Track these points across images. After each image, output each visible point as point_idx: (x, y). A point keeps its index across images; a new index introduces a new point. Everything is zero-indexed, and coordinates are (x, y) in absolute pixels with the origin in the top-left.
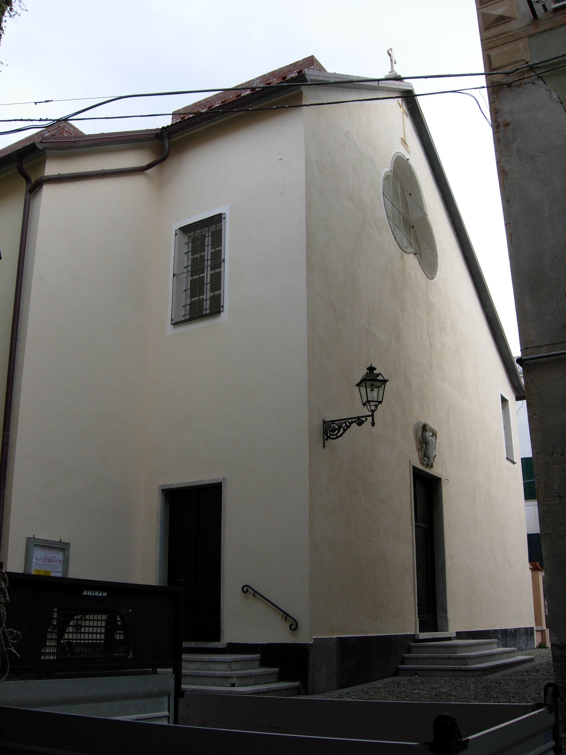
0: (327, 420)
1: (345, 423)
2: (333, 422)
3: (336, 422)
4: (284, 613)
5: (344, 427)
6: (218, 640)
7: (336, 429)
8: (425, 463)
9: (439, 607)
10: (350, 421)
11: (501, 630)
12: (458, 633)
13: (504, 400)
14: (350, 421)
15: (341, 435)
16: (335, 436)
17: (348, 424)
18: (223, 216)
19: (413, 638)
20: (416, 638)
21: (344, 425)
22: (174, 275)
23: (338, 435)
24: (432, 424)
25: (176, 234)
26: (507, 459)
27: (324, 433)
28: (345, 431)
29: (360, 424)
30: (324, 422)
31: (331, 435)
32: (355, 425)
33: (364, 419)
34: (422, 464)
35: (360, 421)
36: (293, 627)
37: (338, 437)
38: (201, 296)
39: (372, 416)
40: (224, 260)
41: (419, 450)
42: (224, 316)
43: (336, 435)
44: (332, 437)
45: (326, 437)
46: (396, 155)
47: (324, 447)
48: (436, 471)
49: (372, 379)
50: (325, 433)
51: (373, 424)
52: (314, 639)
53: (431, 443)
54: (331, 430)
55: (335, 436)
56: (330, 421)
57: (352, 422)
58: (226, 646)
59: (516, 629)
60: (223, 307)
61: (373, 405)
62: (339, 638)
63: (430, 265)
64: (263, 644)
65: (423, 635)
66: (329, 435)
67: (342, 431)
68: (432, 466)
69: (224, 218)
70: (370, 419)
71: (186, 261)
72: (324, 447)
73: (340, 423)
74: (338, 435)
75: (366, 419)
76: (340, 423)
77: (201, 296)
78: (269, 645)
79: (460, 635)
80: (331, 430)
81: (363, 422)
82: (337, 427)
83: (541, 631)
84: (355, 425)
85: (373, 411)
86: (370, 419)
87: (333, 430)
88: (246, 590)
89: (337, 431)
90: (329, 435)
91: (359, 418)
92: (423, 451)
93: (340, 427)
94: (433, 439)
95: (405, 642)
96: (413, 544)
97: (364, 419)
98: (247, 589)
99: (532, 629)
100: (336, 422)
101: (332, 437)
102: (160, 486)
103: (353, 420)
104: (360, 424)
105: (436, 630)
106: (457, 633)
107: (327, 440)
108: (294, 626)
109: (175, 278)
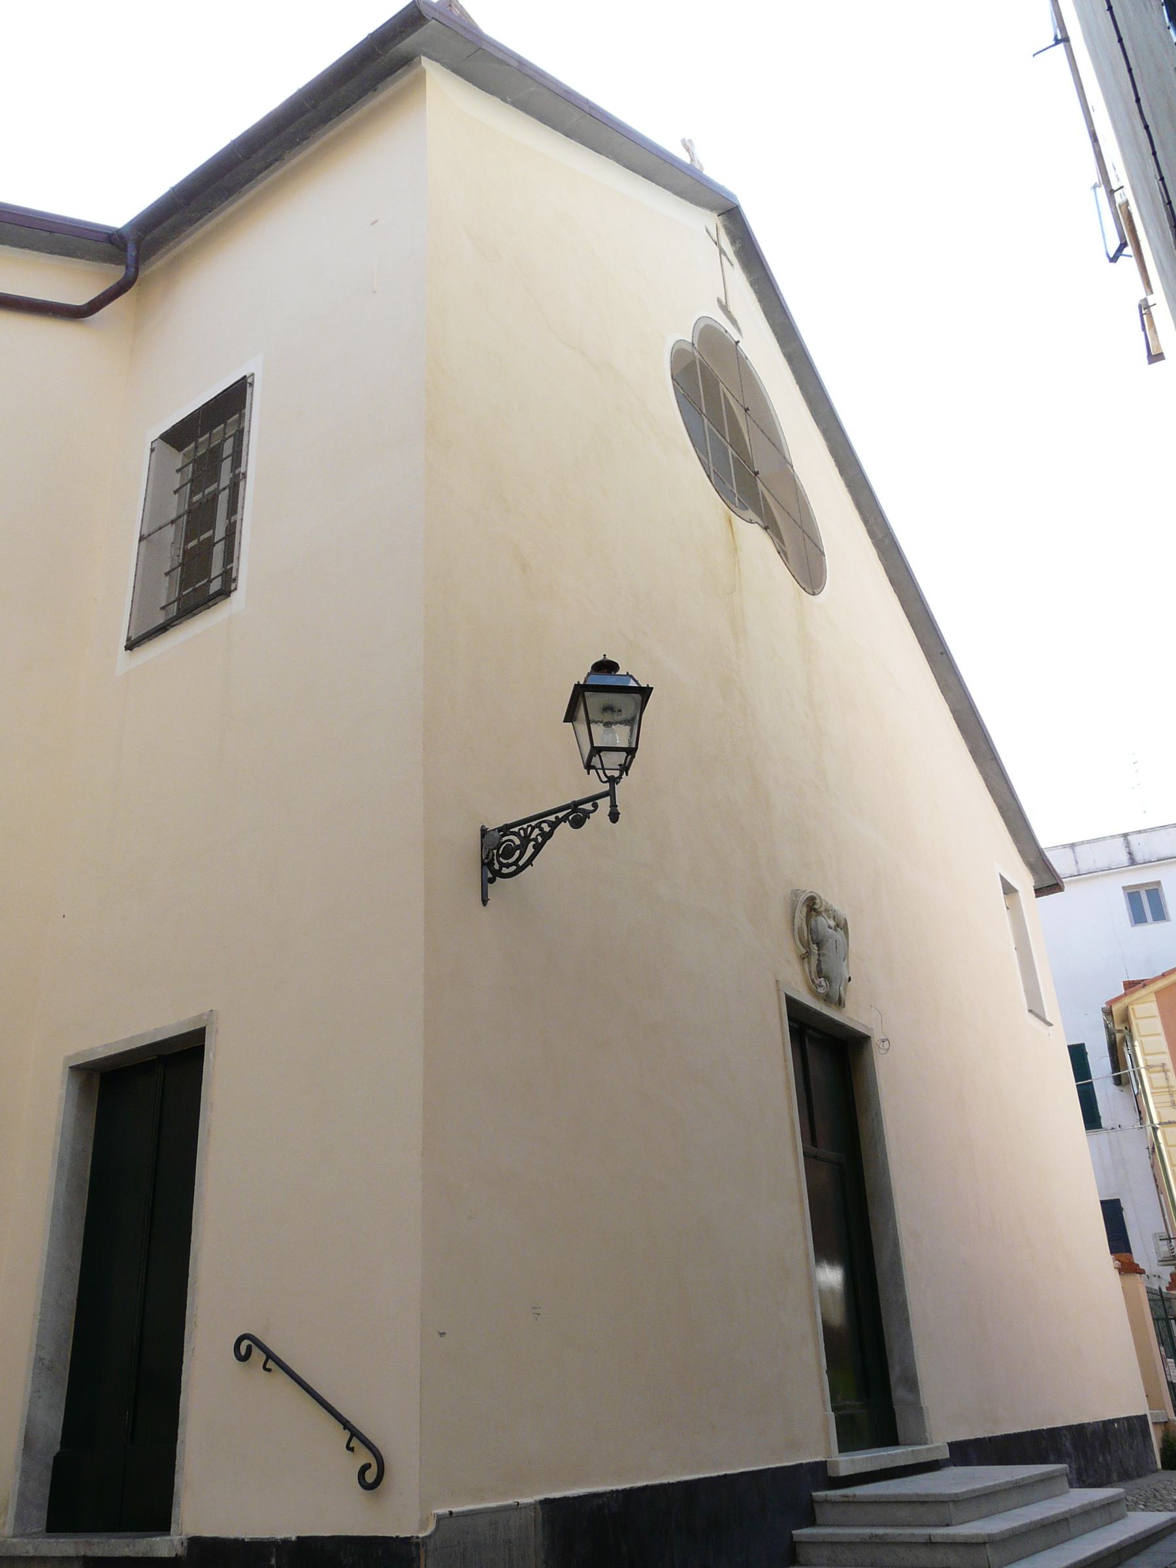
0: (491, 826)
1: (539, 826)
2: (505, 829)
3: (516, 829)
4: (346, 1424)
5: (535, 840)
6: (162, 1523)
7: (518, 847)
8: (821, 990)
9: (895, 1373)
10: (552, 818)
11: (1070, 1428)
12: (952, 1446)
13: (1009, 890)
14: (552, 818)
15: (529, 862)
16: (514, 868)
17: (546, 828)
18: (249, 380)
19: (819, 1474)
20: (831, 1473)
21: (537, 831)
22: (141, 539)
23: (521, 863)
24: (830, 897)
25: (152, 450)
26: (1030, 1011)
27: (483, 864)
28: (538, 848)
29: (578, 823)
30: (484, 832)
31: (502, 865)
32: (565, 827)
33: (588, 806)
34: (816, 994)
35: (576, 814)
36: (370, 1476)
37: (520, 869)
38: (194, 567)
39: (611, 793)
40: (245, 475)
41: (805, 957)
42: (238, 599)
43: (516, 863)
44: (505, 870)
45: (490, 875)
46: (702, 325)
47: (485, 902)
48: (854, 1016)
49: (607, 694)
50: (486, 864)
51: (614, 816)
52: (440, 1519)
53: (830, 944)
54: (503, 854)
55: (514, 868)
56: (500, 830)
57: (559, 821)
58: (180, 1551)
59: (1105, 1423)
60: (235, 580)
61: (611, 764)
62: (546, 1502)
63: (809, 570)
64: (285, 1541)
65: (848, 1463)
66: (497, 866)
67: (530, 850)
68: (840, 1003)
69: (251, 385)
70: (604, 803)
71: (174, 507)
72: (485, 902)
73: (525, 830)
74: (521, 863)
75: (596, 806)
76: (525, 830)
77: (194, 567)
78: (304, 1543)
79: (966, 1453)
80: (503, 854)
81: (587, 814)
82: (517, 842)
83: (1166, 1423)
84: (565, 827)
85: (613, 781)
86: (604, 803)
87: (508, 853)
88: (247, 1348)
89: (518, 852)
90: (497, 866)
91: (574, 806)
92: (814, 961)
93: (526, 840)
94: (839, 935)
95: (790, 1493)
96: (801, 1201)
97: (588, 806)
98: (249, 1348)
99: (1143, 1418)
100: (516, 829)
101: (505, 870)
102: (68, 1058)
103: (560, 815)
104: (578, 823)
105: (892, 1439)
106: (951, 1445)
107: (492, 881)
108: (373, 1478)
109: (144, 543)
